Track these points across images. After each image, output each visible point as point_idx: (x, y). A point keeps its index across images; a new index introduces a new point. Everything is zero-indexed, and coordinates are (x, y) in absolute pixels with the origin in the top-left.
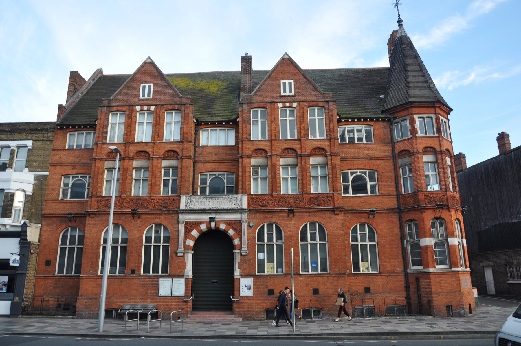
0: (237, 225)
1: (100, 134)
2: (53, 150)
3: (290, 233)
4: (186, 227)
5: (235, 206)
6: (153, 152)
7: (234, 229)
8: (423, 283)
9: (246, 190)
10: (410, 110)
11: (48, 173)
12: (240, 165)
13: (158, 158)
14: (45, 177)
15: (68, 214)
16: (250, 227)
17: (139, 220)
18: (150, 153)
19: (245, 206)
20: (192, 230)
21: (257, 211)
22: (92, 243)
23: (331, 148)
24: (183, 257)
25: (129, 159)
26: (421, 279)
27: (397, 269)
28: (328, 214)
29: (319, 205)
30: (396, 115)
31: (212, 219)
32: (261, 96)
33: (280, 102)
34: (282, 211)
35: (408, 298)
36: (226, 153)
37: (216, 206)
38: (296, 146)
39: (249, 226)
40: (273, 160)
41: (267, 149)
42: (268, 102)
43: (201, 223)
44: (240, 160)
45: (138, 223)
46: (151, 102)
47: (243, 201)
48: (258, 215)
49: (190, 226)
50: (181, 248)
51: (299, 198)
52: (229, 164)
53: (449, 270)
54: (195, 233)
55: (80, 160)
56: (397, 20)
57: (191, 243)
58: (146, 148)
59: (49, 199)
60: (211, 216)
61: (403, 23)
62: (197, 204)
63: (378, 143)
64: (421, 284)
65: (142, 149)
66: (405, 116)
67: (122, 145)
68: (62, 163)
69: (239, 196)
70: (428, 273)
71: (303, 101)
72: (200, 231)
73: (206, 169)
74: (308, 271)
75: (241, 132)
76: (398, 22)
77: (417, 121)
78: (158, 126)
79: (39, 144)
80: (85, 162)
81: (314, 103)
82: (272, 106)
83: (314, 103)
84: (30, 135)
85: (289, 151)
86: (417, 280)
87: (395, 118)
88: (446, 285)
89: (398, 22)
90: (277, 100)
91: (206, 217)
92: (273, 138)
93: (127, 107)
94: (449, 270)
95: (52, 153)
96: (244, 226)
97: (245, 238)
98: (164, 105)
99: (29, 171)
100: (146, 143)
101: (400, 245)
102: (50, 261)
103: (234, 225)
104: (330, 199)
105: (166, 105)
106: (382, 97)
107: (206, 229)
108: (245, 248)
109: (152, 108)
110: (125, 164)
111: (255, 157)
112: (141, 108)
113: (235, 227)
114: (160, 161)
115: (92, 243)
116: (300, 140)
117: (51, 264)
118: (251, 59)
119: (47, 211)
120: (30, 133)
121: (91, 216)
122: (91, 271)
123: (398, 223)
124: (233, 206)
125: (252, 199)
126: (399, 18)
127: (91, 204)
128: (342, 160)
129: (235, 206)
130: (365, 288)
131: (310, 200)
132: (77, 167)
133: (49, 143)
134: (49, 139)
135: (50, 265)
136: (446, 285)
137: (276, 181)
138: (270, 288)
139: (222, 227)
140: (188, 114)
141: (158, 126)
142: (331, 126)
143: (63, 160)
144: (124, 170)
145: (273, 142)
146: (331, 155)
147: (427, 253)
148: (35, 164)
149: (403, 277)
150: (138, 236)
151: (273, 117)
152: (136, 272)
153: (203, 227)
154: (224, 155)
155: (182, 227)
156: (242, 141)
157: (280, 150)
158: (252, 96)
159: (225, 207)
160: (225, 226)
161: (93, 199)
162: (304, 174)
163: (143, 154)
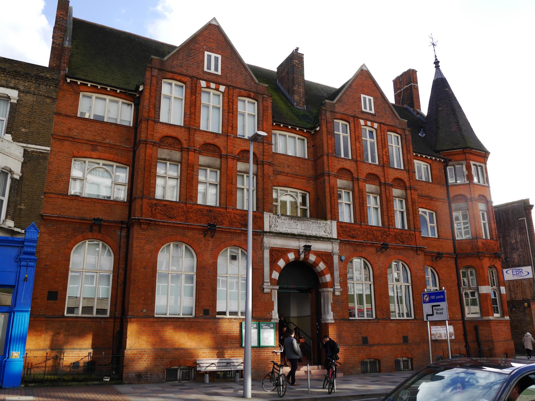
0: (326, 257)
1: (152, 106)
2: (58, 114)
3: (380, 272)
4: (271, 255)
5: (324, 234)
6: (226, 148)
7: (325, 263)
8: (483, 332)
9: (334, 216)
10: (467, 155)
11: (49, 149)
12: (327, 184)
13: (234, 158)
14: (43, 156)
15: (81, 219)
16: (341, 260)
17: (211, 239)
18: (222, 148)
19: (335, 236)
20: (278, 260)
21: (348, 243)
22: (145, 268)
23: (410, 182)
24: (270, 294)
25: (195, 151)
26: (480, 328)
27: (457, 316)
28: (411, 253)
29: (403, 243)
30: (450, 158)
31: (307, 248)
32: (343, 106)
33: (362, 119)
34: (372, 245)
35: (467, 346)
36: (300, 167)
37: (305, 231)
38: (378, 172)
39: (340, 260)
40: (360, 184)
41: (353, 170)
42: (351, 116)
43: (289, 250)
44: (327, 178)
45: (211, 243)
46: (220, 80)
47: (330, 229)
48: (347, 246)
49: (277, 253)
50: (267, 282)
51: (385, 232)
52: (304, 181)
53: (502, 319)
54: (281, 263)
55: (104, 139)
56: (434, 61)
57: (276, 275)
58: (216, 141)
59: (52, 191)
60: (308, 244)
61: (439, 64)
62: (284, 226)
63: (436, 184)
64: (480, 332)
65: (210, 141)
66: (461, 160)
67: (183, 129)
68: (72, 138)
69: (329, 222)
70: (489, 321)
71: (383, 124)
72: (286, 260)
73: (278, 183)
74: (364, 317)
75: (326, 145)
76: (435, 63)
77: (473, 167)
78: (231, 115)
79: (29, 98)
80: (112, 142)
81: (393, 129)
82: (356, 122)
83: (393, 129)
84: (13, 81)
85: (372, 177)
86: (476, 329)
87: (450, 160)
88: (502, 333)
89: (435, 63)
90: (359, 116)
91: (299, 244)
92: (359, 159)
93: (188, 78)
94: (502, 319)
95: (55, 118)
96: (336, 259)
97: (337, 274)
98: (237, 88)
99: (14, 140)
100: (216, 135)
101: (457, 291)
102: (57, 292)
103: (324, 258)
104: (412, 236)
105: (239, 88)
106: (318, 129)
107: (293, 260)
108: (337, 286)
109: (222, 88)
110: (190, 158)
111: (341, 178)
112: (207, 84)
113: (326, 260)
114: (235, 161)
115: (145, 268)
116: (383, 166)
117: (59, 297)
118: (303, 58)
119: (48, 211)
120: (14, 77)
121: (143, 226)
122: (145, 311)
123: (455, 269)
124: (322, 234)
125: (341, 226)
126: (436, 59)
127: (142, 209)
128: (420, 196)
129: (324, 234)
130: (403, 337)
131: (396, 236)
132: (100, 148)
133: (48, 101)
134: (50, 95)
135: (56, 299)
136: (502, 333)
137: (364, 209)
138: (364, 335)
139: (312, 258)
140: (267, 107)
141: (231, 115)
142: (409, 157)
143: (75, 133)
144: (188, 166)
145: (358, 163)
146: (410, 188)
147: (487, 301)
148: (23, 130)
149: (461, 325)
150: (211, 261)
151: (357, 134)
152: (210, 313)
153: (291, 256)
154: (297, 168)
155: (267, 254)
156: (328, 156)
157: (365, 174)
158: (334, 104)
159: (314, 234)
160: (315, 257)
161: (145, 200)
162: (389, 205)
163: (211, 148)
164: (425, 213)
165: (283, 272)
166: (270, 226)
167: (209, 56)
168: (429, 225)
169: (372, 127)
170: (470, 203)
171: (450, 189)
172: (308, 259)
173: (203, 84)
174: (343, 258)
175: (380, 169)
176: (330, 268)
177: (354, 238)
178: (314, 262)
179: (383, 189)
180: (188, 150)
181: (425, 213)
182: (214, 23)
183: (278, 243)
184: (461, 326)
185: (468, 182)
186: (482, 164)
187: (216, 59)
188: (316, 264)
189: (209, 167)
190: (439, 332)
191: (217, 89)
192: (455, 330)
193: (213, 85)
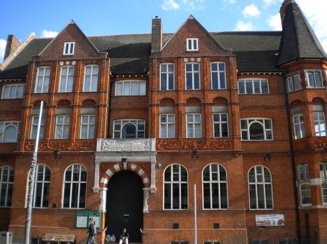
0: (146, 166)
7: (144, 170)
8: (312, 219)
12: (150, 112)
26: (310, 215)
27: (289, 206)
31: (124, 160)
33: (186, 58)
35: (298, 232)
39: (157, 167)
41: (174, 98)
43: (115, 163)
45: (60, 163)
54: (109, 172)
63: (273, 95)
70: (317, 210)
86: (307, 216)
90: (183, 56)
96: (153, 166)
97: (153, 176)
100: (68, 94)
116: (204, 90)
139: (133, 167)
153: (117, 167)
164: (261, 121)
165: (111, 180)
166: (102, 148)
167: (190, 42)
168: (265, 130)
169: (196, 61)
170: (229, 106)
171: (289, 97)
172: (130, 168)
173: (62, 63)
174: (160, 165)
175: (200, 93)
176: (148, 174)
177: (167, 151)
178: (135, 170)
179: (202, 108)
180: (231, 104)
181: (261, 121)
182: (192, 18)
183: (107, 159)
184: (294, 214)
185: (302, 88)
186: (318, 70)
187: (195, 41)
188: (137, 170)
189: (64, 115)
190: (268, 220)
191: (71, 64)
192: (285, 218)
193: (68, 63)
